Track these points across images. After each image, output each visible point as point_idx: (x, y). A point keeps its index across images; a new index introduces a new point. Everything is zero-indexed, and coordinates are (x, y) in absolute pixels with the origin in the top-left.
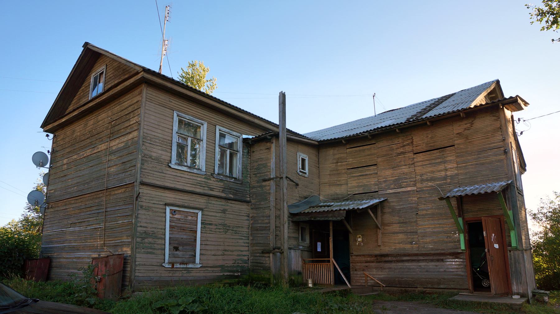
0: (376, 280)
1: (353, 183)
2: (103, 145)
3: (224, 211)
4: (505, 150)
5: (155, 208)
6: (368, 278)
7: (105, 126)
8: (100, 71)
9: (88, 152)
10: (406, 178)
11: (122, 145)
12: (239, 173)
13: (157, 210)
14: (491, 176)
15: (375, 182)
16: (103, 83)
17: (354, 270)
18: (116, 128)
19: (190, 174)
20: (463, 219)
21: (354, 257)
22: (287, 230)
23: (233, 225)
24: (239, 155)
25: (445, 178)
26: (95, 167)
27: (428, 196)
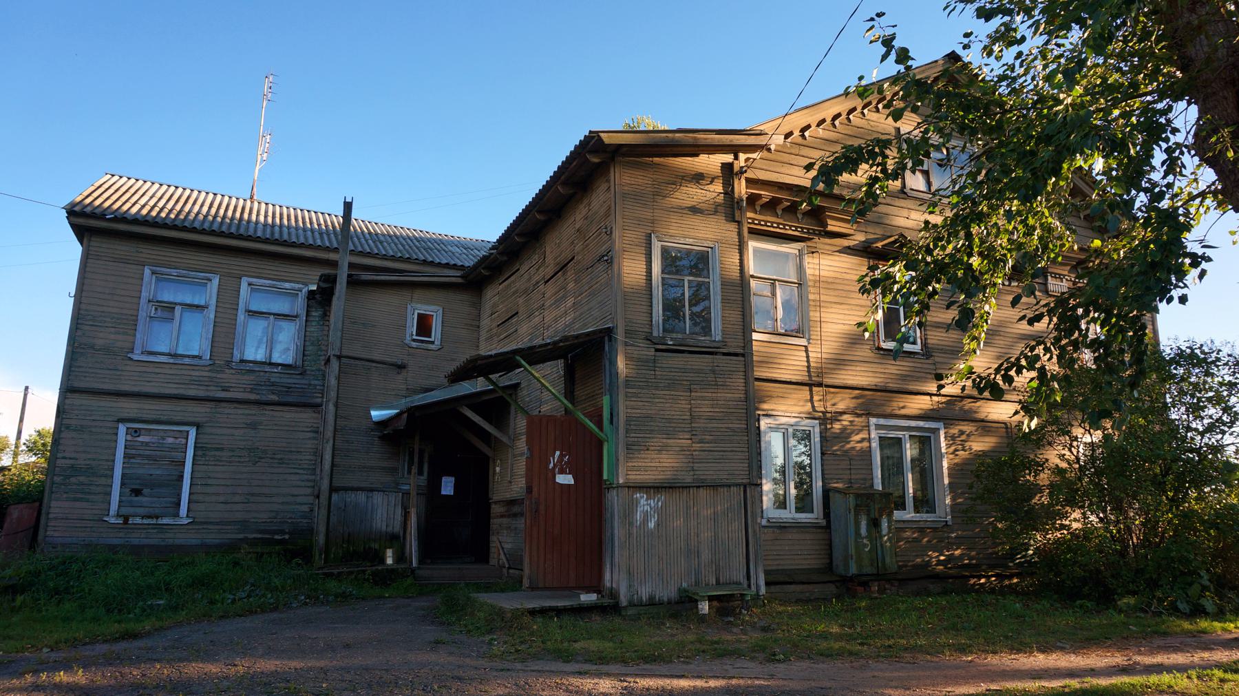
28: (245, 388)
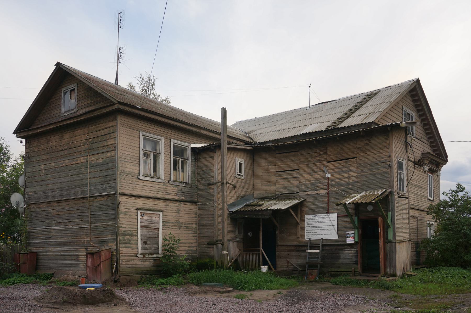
0: (295, 265)
1: (280, 184)
2: (82, 158)
3: (178, 211)
4: (390, 164)
5: (130, 212)
6: (289, 264)
7: (82, 141)
8: (70, 87)
9: (67, 162)
10: (320, 183)
11: (101, 161)
12: (188, 178)
13: (131, 214)
14: (379, 184)
15: (297, 184)
16: (75, 100)
17: (279, 257)
18: (94, 146)
19: (153, 183)
20: (358, 218)
21: (279, 247)
22: (227, 225)
23: (185, 222)
24: (189, 163)
25: (348, 184)
26: (76, 176)
27: (335, 198)
28: (175, 194)
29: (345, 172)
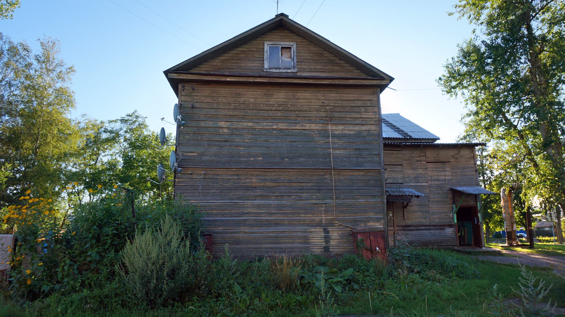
10: (422, 177)
25: (445, 180)
29: (442, 171)
